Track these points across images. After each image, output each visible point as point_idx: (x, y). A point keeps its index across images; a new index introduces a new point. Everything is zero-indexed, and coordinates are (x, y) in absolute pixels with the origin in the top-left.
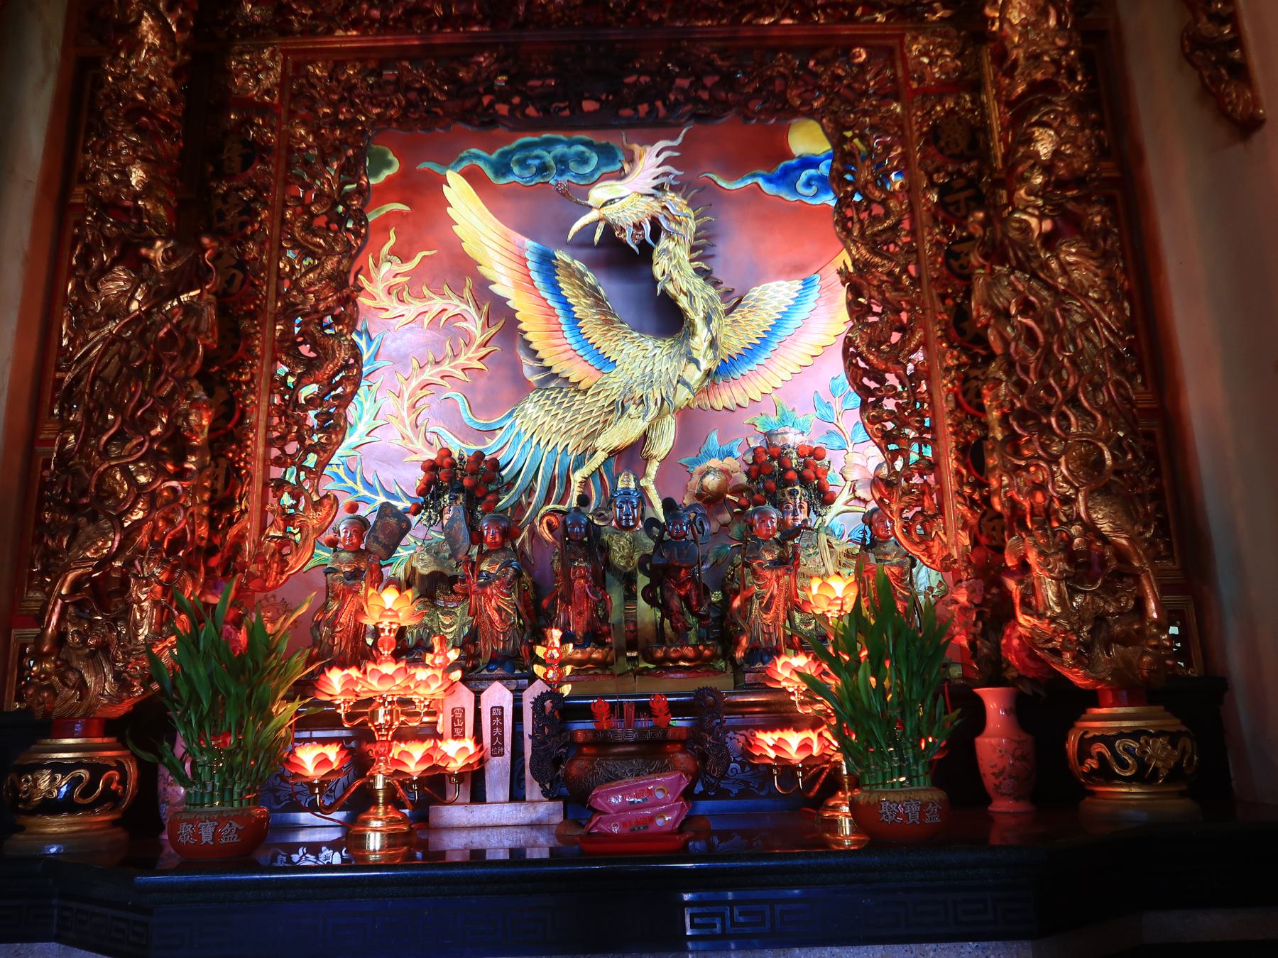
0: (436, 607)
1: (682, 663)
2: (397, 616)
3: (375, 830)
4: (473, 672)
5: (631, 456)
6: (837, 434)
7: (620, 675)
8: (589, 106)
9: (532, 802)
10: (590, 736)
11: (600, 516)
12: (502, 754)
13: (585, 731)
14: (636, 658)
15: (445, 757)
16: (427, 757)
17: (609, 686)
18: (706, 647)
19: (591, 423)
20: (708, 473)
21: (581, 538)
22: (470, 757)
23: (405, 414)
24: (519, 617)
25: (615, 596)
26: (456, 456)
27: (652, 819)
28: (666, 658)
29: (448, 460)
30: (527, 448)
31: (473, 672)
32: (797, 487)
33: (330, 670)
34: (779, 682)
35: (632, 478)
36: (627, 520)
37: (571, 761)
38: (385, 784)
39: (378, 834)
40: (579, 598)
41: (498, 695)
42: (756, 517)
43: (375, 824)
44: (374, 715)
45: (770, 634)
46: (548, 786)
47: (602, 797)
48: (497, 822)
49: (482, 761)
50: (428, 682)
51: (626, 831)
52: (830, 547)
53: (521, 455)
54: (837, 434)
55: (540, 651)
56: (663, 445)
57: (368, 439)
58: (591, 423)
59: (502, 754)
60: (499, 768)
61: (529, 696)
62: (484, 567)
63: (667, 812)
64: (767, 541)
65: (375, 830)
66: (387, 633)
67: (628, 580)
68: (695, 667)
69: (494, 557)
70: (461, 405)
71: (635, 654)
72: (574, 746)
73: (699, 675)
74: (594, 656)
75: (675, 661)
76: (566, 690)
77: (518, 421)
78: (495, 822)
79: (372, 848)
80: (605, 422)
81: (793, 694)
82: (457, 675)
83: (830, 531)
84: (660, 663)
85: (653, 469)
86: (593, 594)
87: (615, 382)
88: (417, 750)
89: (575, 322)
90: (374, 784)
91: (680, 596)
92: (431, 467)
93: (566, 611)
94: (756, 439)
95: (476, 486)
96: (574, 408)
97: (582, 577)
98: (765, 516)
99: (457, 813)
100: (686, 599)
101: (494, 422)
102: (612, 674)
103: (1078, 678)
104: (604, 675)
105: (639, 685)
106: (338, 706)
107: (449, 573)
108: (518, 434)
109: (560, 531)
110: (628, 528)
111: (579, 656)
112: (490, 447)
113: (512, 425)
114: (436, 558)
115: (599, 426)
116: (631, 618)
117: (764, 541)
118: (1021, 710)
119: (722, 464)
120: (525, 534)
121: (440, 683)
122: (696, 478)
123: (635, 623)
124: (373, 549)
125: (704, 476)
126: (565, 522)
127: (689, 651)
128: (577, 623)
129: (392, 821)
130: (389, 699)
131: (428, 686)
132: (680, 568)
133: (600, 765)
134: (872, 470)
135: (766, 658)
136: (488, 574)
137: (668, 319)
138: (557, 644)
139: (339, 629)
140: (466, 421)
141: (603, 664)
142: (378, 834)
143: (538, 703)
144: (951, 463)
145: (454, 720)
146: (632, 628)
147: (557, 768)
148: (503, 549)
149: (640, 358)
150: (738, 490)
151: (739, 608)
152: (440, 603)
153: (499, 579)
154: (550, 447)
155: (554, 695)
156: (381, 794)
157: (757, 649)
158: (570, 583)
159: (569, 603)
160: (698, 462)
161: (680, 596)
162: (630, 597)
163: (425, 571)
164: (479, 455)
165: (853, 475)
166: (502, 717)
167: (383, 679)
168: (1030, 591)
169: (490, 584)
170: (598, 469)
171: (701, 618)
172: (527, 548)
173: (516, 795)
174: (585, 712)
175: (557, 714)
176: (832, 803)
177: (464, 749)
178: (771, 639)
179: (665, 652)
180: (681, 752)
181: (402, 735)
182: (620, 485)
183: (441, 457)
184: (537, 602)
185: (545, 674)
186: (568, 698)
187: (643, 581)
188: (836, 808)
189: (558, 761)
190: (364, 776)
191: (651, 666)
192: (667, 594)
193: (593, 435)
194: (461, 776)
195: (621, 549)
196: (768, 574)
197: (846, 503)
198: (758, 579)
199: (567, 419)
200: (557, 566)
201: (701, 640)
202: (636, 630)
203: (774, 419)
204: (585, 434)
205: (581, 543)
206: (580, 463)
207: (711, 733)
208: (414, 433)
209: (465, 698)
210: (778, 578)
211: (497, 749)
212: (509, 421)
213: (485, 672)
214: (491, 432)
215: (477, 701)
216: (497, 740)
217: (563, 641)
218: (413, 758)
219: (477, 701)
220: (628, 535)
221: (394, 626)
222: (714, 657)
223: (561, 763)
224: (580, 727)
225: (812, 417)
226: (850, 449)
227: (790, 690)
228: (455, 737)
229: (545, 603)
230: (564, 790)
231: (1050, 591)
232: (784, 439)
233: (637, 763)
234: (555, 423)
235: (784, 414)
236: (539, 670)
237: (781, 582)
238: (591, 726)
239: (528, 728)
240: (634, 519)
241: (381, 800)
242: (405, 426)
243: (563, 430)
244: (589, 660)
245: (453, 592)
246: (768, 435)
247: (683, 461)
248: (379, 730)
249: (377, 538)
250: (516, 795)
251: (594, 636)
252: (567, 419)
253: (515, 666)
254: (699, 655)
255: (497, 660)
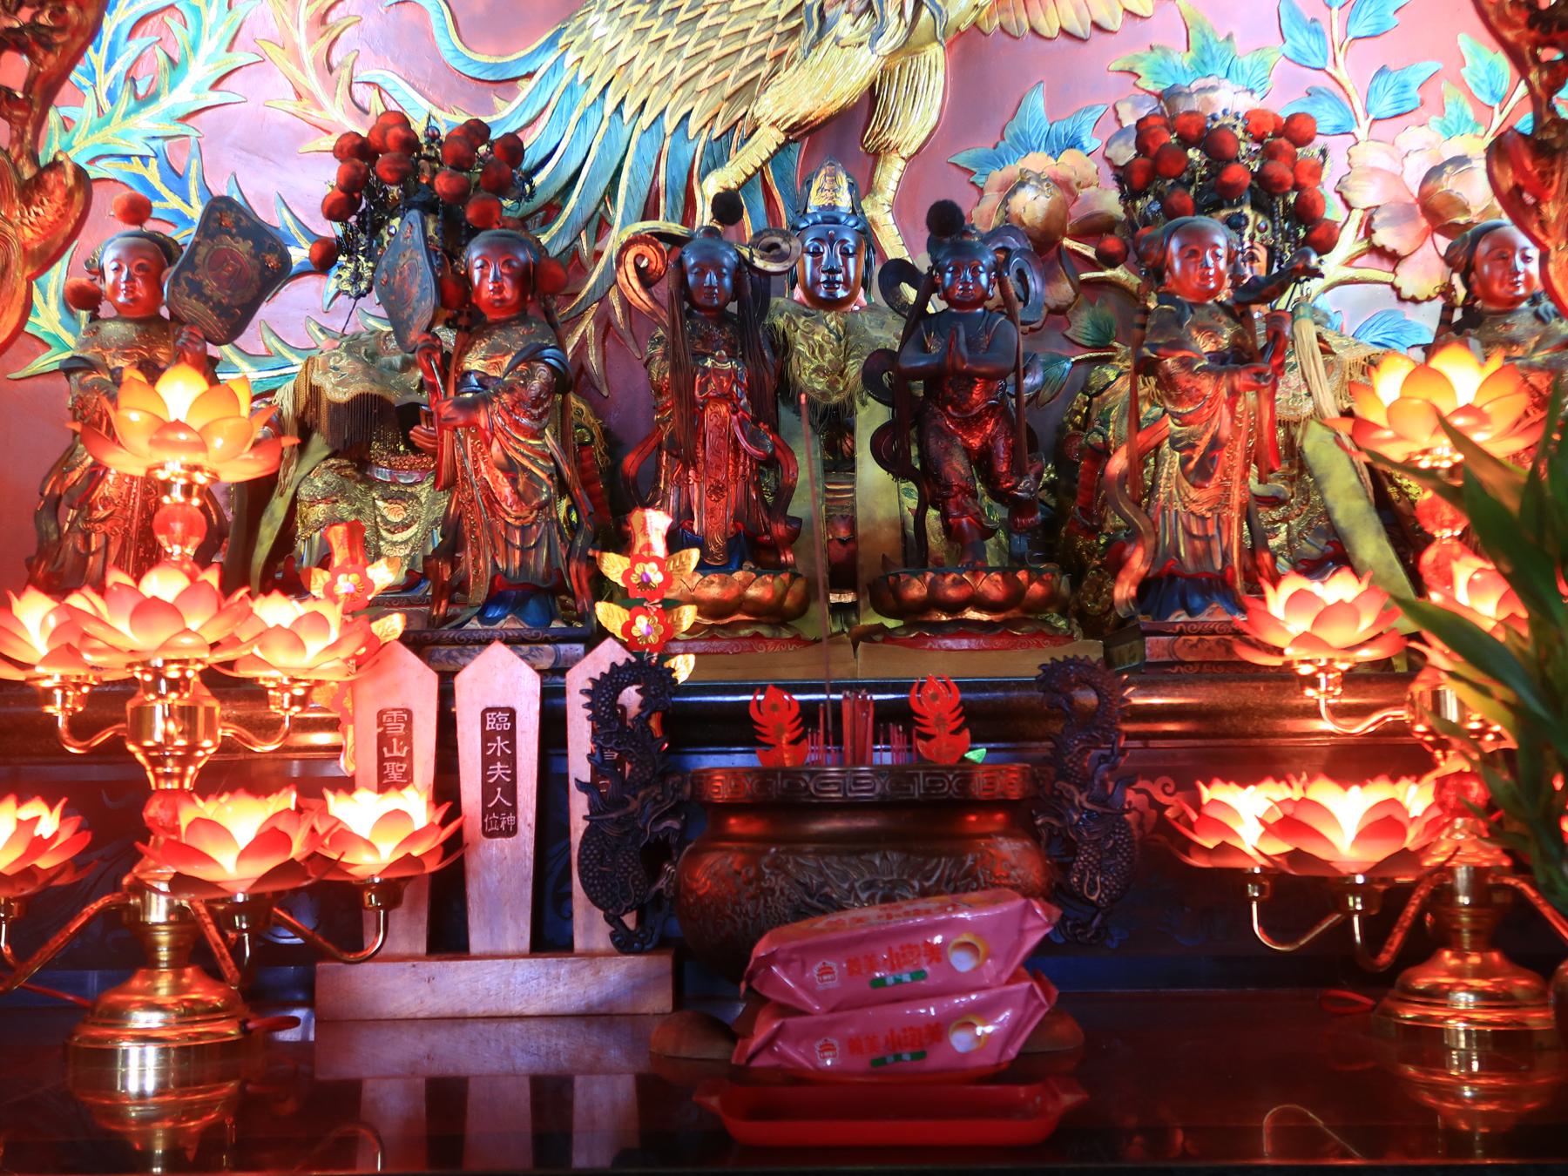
0: (371, 483)
1: (972, 615)
2: (202, 446)
3: (144, 1038)
4: (440, 614)
5: (844, 135)
6: (1331, 97)
7: (583, 955)
9: (590, 955)
10: (749, 784)
11: (771, 251)
12: (511, 831)
13: (733, 772)
14: (852, 607)
15: (343, 836)
16: (271, 838)
17: (792, 665)
18: (1036, 576)
19: (745, 60)
20: (1022, 184)
21: (720, 302)
22: (415, 837)
23: (300, 38)
24: (563, 488)
25: (806, 458)
26: (419, 128)
27: (937, 1031)
28: (934, 602)
29: (398, 131)
30: (594, 118)
31: (440, 614)
32: (1247, 211)
33: (19, 594)
34: (1280, 652)
35: (843, 181)
36: (831, 284)
37: (695, 854)
38: (173, 910)
39: (152, 1050)
40: (716, 452)
41: (501, 679)
42: (1174, 245)
43: (144, 1020)
44: (142, 719)
45: (1207, 539)
46: (630, 920)
47: (785, 964)
48: (507, 993)
49: (454, 846)
50: (298, 642)
51: (860, 1063)
52: (1326, 351)
53: (576, 137)
54: (1331, 97)
55: (614, 566)
56: (914, 122)
57: (214, 98)
58: (745, 60)
59: (511, 831)
60: (503, 866)
61: (579, 679)
62: (474, 362)
63: (985, 1011)
64: (1201, 305)
65: (144, 1038)
66: (177, 495)
67: (835, 425)
68: (1006, 623)
69: (498, 338)
70: (434, 18)
71: (848, 598)
72: (703, 814)
73: (1016, 643)
74: (752, 592)
75: (956, 607)
76: (683, 667)
77: (571, 57)
78: (492, 1007)
79: (133, 1087)
80: (778, 58)
81: (1312, 681)
82: (392, 625)
83: (1321, 319)
84: (914, 614)
85: (890, 175)
86: (754, 439)
88: (243, 817)
90: (145, 908)
91: (968, 450)
92: (357, 151)
93: (682, 483)
94: (1137, 105)
95: (462, 196)
96: (704, 23)
97: (725, 397)
98: (1196, 244)
99: (401, 984)
100: (982, 461)
101: (513, 59)
102: (798, 640)
104: (776, 640)
105: (862, 665)
106: (47, 696)
107: (397, 398)
108: (570, 88)
109: (664, 289)
110: (832, 304)
111: (714, 591)
112: (503, 117)
113: (555, 67)
114: (368, 366)
115: (764, 70)
116: (843, 513)
117: (1192, 306)
119: (1055, 164)
120: (587, 326)
121: (334, 634)
122: (992, 199)
123: (852, 523)
124: (185, 314)
125: (1014, 192)
126: (680, 262)
127: (992, 586)
128: (711, 513)
129: (191, 1013)
130: (173, 672)
131: (298, 644)
132: (969, 378)
133: (777, 867)
134: (1413, 180)
135: (1196, 601)
136: (484, 380)
138: (660, 549)
139: (101, 513)
140: (448, 56)
141: (774, 615)
142: (152, 1050)
143: (604, 691)
145: (383, 740)
146: (843, 533)
147: (655, 872)
148: (523, 319)
150: (1094, 229)
151: (1124, 477)
152: (382, 474)
153: (510, 390)
154: (646, 120)
155: (645, 668)
156: (163, 937)
157: (1172, 576)
158: (693, 413)
159: (689, 461)
160: (999, 161)
161: (968, 450)
162: (840, 463)
163: (342, 395)
164: (477, 131)
165: (1366, 195)
166: (511, 735)
167: (154, 623)
169: (487, 401)
170: (759, 170)
171: (1018, 507)
172: (593, 359)
173: (549, 938)
174: (735, 727)
175: (658, 731)
176: (1422, 983)
177: (398, 815)
178: (1209, 552)
179: (932, 587)
180: (1008, 834)
181: (230, 774)
182: (816, 201)
183: (381, 129)
184: (613, 470)
185: (627, 627)
186: (688, 689)
187: (871, 416)
188: (1437, 995)
189: (657, 854)
190: (116, 886)
191: (891, 623)
192: (935, 445)
193: (747, 91)
194: (391, 889)
195: (814, 352)
196: (1207, 385)
197: (1349, 263)
198: (1178, 401)
199: (687, 52)
200: (660, 370)
201: (1013, 562)
202: (853, 539)
203: (1182, 59)
204: (729, 89)
205: (720, 316)
206: (717, 156)
207: (1084, 784)
208: (324, 82)
209: (415, 684)
210: (1234, 394)
211: (499, 819)
212: (549, 58)
213: (474, 625)
214: (507, 84)
215: (446, 696)
216: (500, 794)
217: (676, 540)
218: (233, 839)
219: (446, 696)
220: (832, 319)
221: (200, 478)
222: (1051, 599)
223: (668, 857)
224: (722, 765)
225: (1275, 54)
226: (1361, 133)
227: (1305, 670)
228: (384, 785)
229: (630, 462)
230: (675, 926)
232: (1209, 103)
233: (887, 862)
234: (658, 59)
235: (1205, 49)
236: (609, 614)
237: (1240, 408)
238: (740, 760)
239: (579, 766)
240: (846, 283)
241: (164, 954)
242: (301, 67)
243: (678, 78)
244: (741, 603)
245: (410, 445)
246: (1167, 96)
247: (961, 159)
248: (156, 762)
249: (203, 284)
250: (549, 938)
251: (749, 545)
252: (687, 52)
253: (549, 608)
254: (1016, 596)
255: (505, 595)
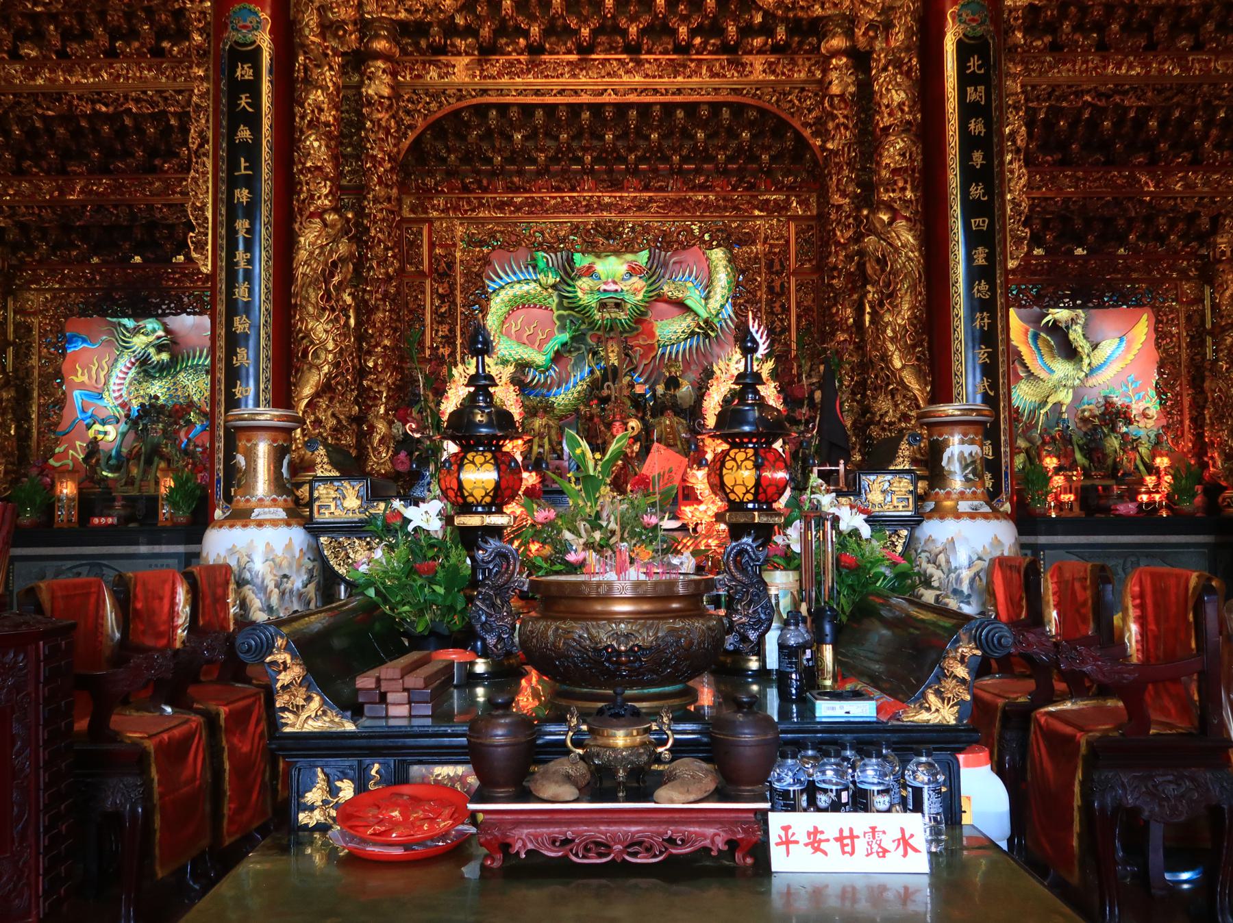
8: (1079, 302)
87: (1055, 377)
89: (1039, 350)
103: (1224, 484)
118: (1206, 492)
119: (1092, 406)
137: (1071, 353)
144: (1187, 422)
149: (1062, 368)
168: (1215, 463)
231: (1219, 463)
